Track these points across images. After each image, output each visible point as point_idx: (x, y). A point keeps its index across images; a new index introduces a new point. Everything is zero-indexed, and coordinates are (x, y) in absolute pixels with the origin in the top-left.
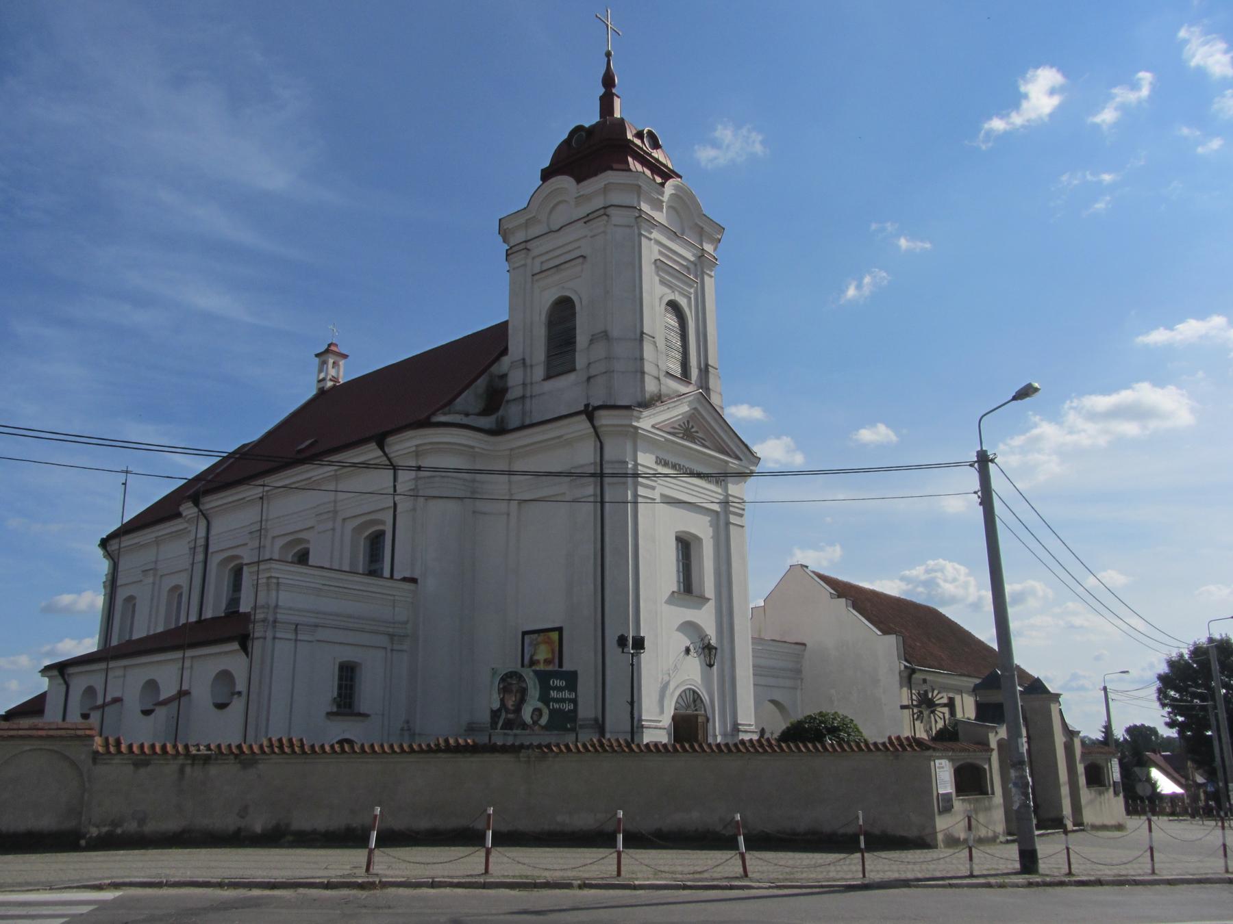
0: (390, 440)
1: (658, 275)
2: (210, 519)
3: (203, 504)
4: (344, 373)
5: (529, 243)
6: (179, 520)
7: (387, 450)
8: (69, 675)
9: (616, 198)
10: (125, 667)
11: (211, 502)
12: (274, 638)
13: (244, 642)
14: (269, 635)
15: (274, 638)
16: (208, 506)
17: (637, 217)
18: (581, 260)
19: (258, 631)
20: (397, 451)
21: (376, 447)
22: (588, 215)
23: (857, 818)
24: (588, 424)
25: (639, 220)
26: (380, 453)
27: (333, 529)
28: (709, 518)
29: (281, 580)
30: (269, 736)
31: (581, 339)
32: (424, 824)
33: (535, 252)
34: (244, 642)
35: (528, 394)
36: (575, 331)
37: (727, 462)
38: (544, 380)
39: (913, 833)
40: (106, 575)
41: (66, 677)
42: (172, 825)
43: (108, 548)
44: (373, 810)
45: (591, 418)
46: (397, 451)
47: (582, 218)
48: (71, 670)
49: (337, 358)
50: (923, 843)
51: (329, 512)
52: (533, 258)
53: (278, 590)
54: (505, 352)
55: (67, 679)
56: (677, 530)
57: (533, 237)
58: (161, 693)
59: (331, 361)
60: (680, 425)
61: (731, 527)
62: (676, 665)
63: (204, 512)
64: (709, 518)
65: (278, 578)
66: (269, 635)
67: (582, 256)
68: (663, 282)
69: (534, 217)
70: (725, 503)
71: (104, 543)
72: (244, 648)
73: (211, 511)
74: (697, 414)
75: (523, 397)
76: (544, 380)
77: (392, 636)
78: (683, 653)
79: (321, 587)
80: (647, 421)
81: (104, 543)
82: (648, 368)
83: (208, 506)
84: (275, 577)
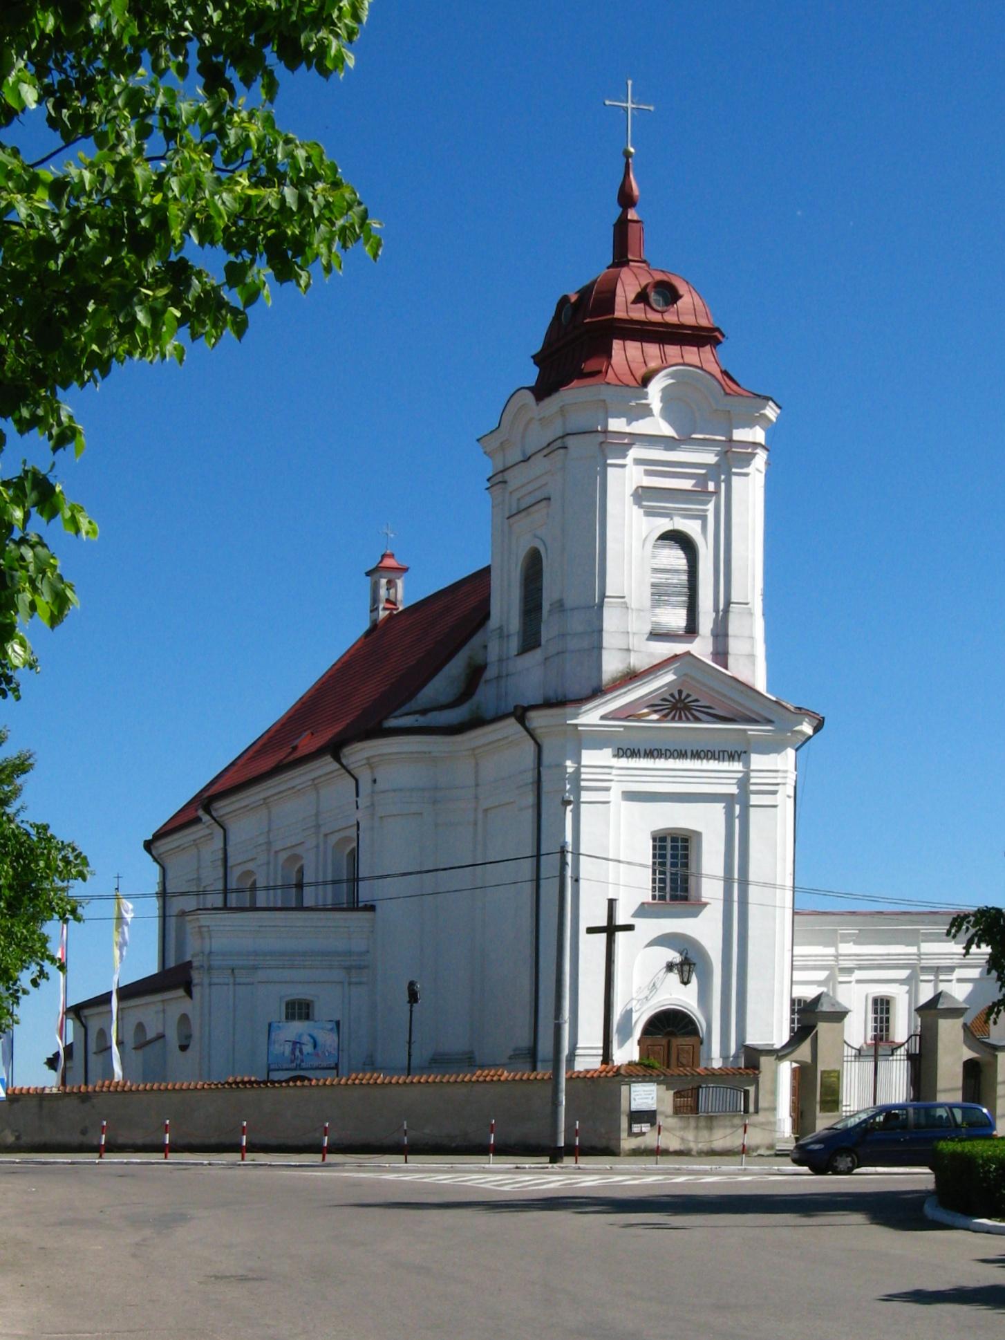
0: (346, 751)
1: (641, 506)
2: (225, 827)
3: (216, 810)
4: (405, 594)
5: (505, 473)
6: (200, 826)
7: (344, 761)
8: (85, 1017)
9: (576, 422)
10: (163, 1001)
11: (223, 808)
12: (210, 984)
13: (188, 988)
14: (206, 981)
15: (210, 984)
16: (222, 812)
17: (602, 443)
18: (544, 504)
19: (196, 976)
20: (356, 762)
21: (332, 760)
22: (549, 445)
23: (403, 1125)
24: (518, 727)
25: (603, 445)
26: (337, 766)
27: (268, 863)
28: (723, 805)
29: (211, 929)
30: (507, 1061)
31: (546, 606)
32: (213, 1140)
33: (512, 485)
34: (188, 988)
35: (504, 674)
36: (542, 593)
37: (745, 731)
38: (519, 654)
39: (602, 1143)
40: (158, 883)
41: (83, 1019)
42: (38, 1139)
43: (154, 852)
44: (102, 1122)
45: (521, 720)
46: (356, 762)
47: (539, 451)
48: (86, 1012)
49: (392, 575)
50: (610, 1150)
51: (193, 879)
52: (511, 493)
53: (210, 938)
54: (487, 616)
55: (84, 1021)
56: (653, 830)
57: (513, 463)
58: (148, 1031)
59: (383, 581)
60: (664, 700)
61: (581, 857)
62: (654, 985)
63: (217, 819)
64: (723, 805)
65: (208, 926)
66: (206, 981)
67: (545, 499)
68: (650, 513)
69: (507, 440)
70: (744, 783)
71: (148, 846)
72: (189, 993)
73: (226, 817)
74: (688, 680)
75: (499, 677)
76: (519, 654)
77: (348, 969)
78: (665, 970)
79: (258, 929)
80: (591, 716)
81: (148, 846)
82: (607, 640)
83: (222, 812)
84: (205, 926)
